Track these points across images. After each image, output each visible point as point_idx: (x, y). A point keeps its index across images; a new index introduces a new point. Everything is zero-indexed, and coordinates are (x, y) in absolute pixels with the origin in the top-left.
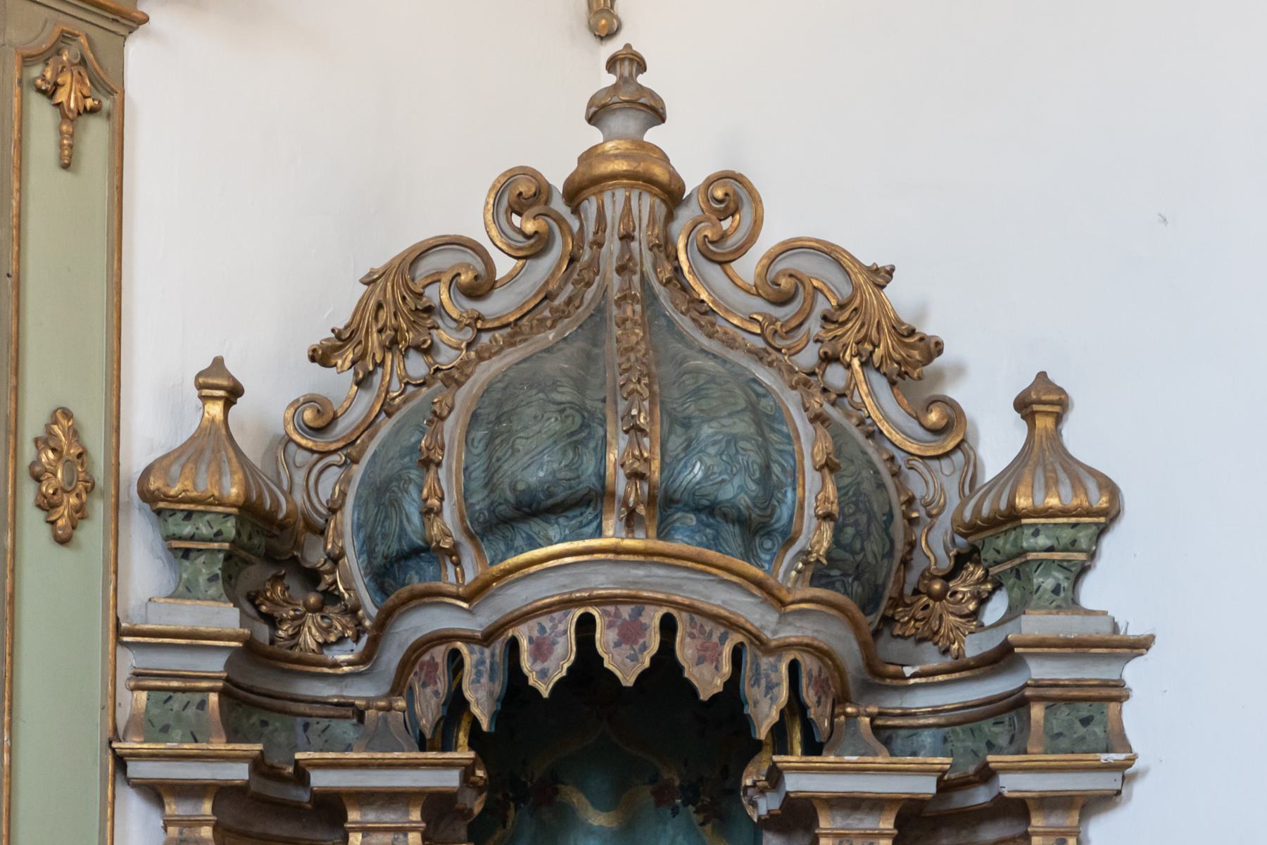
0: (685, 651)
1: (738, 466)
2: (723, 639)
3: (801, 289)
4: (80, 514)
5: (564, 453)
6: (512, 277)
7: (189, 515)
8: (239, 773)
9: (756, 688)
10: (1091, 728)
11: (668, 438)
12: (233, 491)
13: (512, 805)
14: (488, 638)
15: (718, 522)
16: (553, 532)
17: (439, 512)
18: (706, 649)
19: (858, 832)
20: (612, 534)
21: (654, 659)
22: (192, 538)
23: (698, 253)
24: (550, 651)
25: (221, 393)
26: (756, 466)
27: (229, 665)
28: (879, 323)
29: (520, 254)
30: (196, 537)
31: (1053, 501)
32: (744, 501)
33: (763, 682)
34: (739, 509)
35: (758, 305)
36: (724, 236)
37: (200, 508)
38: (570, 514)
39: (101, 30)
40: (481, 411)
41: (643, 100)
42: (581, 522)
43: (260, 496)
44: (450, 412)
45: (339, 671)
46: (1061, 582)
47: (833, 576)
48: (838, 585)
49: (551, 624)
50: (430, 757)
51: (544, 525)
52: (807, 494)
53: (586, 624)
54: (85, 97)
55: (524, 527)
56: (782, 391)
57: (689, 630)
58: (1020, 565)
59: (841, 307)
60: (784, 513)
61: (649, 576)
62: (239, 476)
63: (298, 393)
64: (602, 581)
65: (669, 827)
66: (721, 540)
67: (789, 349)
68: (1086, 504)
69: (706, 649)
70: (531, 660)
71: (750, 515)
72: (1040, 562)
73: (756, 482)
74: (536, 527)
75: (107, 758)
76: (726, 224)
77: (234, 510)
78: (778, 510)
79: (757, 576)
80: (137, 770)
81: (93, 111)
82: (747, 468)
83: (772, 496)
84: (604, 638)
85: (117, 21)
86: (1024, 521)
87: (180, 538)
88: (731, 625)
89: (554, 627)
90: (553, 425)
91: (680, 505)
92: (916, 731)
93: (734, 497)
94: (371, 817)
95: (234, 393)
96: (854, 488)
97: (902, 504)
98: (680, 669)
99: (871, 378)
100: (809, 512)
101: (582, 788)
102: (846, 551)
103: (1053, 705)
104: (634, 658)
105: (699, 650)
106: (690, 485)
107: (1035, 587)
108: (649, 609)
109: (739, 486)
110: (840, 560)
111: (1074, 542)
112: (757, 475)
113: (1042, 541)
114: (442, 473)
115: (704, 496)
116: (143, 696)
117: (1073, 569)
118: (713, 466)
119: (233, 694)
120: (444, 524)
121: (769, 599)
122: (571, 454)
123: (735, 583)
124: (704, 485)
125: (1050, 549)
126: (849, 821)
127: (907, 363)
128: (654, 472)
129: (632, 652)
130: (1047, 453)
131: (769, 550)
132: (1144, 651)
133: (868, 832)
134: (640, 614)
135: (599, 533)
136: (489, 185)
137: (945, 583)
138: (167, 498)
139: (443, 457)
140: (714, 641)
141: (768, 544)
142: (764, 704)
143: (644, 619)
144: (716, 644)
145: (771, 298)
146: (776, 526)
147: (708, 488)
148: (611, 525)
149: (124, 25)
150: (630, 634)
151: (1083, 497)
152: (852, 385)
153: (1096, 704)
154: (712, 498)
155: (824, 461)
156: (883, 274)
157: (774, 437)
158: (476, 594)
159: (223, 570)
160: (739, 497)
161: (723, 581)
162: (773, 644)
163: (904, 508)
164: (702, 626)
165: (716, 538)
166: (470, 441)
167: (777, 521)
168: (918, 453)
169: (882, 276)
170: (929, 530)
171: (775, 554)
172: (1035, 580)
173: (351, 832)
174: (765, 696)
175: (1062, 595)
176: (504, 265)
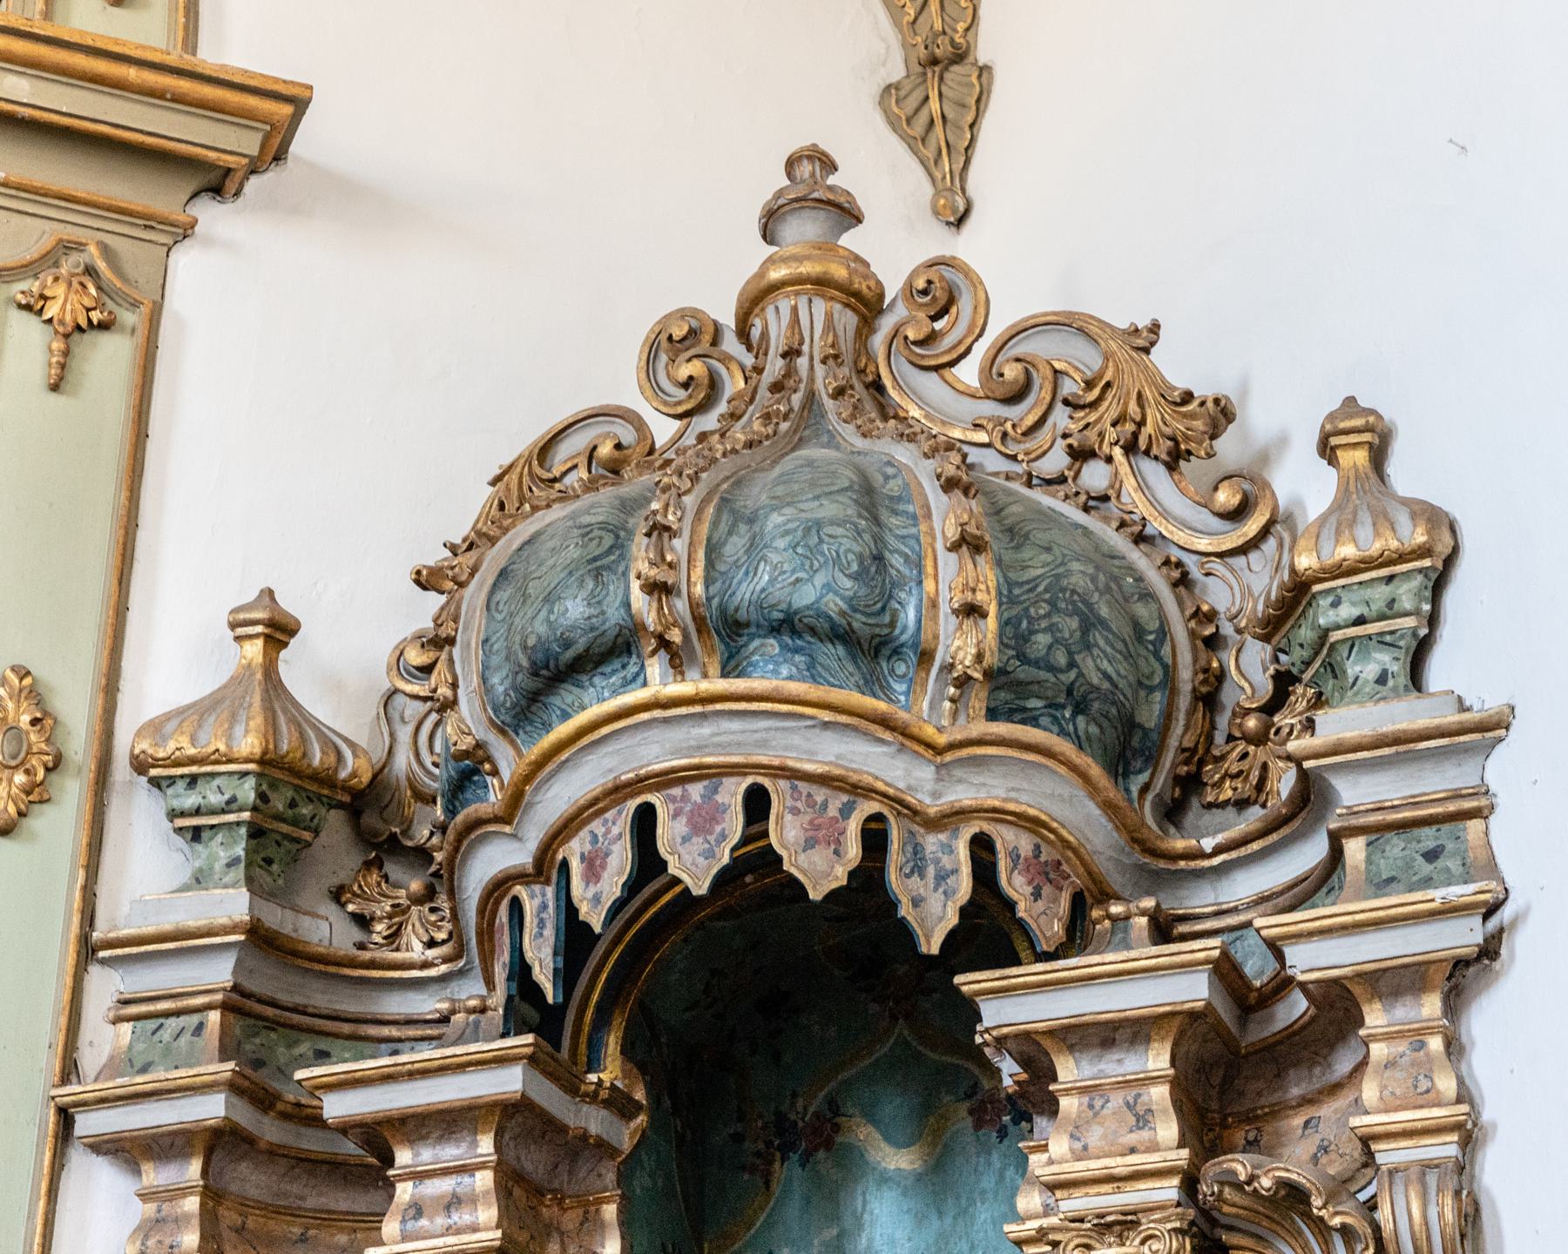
0: (785, 833)
1: (822, 560)
2: (846, 811)
3: (1035, 374)
5: (581, 582)
7: (193, 780)
9: (916, 878)
10: (1440, 863)
11: (726, 541)
12: (249, 743)
13: (778, 1155)
15: (809, 642)
18: (818, 828)
19: (1114, 1079)
22: (198, 812)
23: (915, 371)
24: (603, 867)
25: (259, 629)
26: (851, 556)
27: (239, 965)
28: (1140, 396)
29: (680, 410)
30: (203, 810)
31: (1348, 551)
32: (834, 605)
33: (931, 871)
34: (830, 617)
35: (990, 408)
37: (209, 769)
38: (607, 669)
39: (126, 239)
40: (515, 566)
41: (815, 195)
42: (625, 677)
44: (472, 575)
45: (433, 972)
46: (1388, 666)
47: (1031, 709)
48: (1044, 721)
49: (603, 830)
50: (472, 1050)
51: (576, 690)
52: (940, 587)
53: (645, 821)
54: (88, 310)
55: (556, 700)
56: (916, 464)
57: (789, 803)
58: (1328, 655)
61: (718, 734)
62: (258, 721)
65: (995, 1157)
66: (819, 669)
67: (1027, 454)
68: (1394, 544)
69: (818, 828)
70: (583, 884)
71: (849, 624)
72: (1352, 642)
73: (855, 577)
74: (566, 695)
75: (47, 1114)
76: (938, 325)
77: (252, 767)
78: (902, 615)
79: (876, 710)
80: (88, 1124)
81: (104, 326)
82: (837, 561)
83: (891, 597)
84: (668, 832)
85: (153, 228)
86: (1316, 588)
88: (859, 790)
89: (608, 831)
90: (573, 553)
91: (753, 630)
92: (1239, 933)
93: (817, 601)
94: (428, 1155)
95: (280, 631)
96: (1048, 581)
97: (1189, 620)
98: (893, 905)
99: (1142, 468)
100: (944, 608)
101: (872, 1120)
102: (1039, 668)
103: (1377, 839)
105: (806, 830)
106: (755, 595)
107: (1351, 680)
109: (824, 586)
110: (1032, 683)
112: (855, 567)
113: (1347, 611)
114: (457, 652)
115: (772, 606)
116: (126, 1028)
117: (1402, 643)
118: (782, 563)
119: (238, 1003)
120: (462, 721)
121: (908, 743)
122: (590, 584)
123: (847, 726)
124: (771, 590)
125: (1360, 621)
126: (1102, 1066)
127: (1187, 438)
128: (695, 584)
129: (707, 846)
130: (1354, 496)
131: (904, 676)
132: (1502, 732)
133: (1128, 1077)
134: (716, 791)
136: (643, 338)
137: (1267, 718)
139: (456, 631)
140: (831, 815)
141: (901, 668)
142: (935, 902)
143: (719, 798)
145: (998, 395)
146: (904, 638)
148: (656, 668)
149: (161, 230)
151: (1388, 533)
152: (1116, 482)
153: (1446, 827)
154: (783, 606)
155: (957, 536)
156: (1145, 334)
157: (894, 521)
158: (516, 803)
159: (246, 850)
160: (825, 600)
161: (826, 725)
162: (932, 811)
163: (1192, 624)
164: (809, 795)
165: (811, 666)
166: (493, 606)
167: (902, 633)
168: (1210, 549)
169: (1145, 339)
170: (1239, 651)
171: (911, 679)
172: (1349, 671)
173: (399, 1181)
174: (936, 889)
175: (1391, 683)
176: (663, 429)
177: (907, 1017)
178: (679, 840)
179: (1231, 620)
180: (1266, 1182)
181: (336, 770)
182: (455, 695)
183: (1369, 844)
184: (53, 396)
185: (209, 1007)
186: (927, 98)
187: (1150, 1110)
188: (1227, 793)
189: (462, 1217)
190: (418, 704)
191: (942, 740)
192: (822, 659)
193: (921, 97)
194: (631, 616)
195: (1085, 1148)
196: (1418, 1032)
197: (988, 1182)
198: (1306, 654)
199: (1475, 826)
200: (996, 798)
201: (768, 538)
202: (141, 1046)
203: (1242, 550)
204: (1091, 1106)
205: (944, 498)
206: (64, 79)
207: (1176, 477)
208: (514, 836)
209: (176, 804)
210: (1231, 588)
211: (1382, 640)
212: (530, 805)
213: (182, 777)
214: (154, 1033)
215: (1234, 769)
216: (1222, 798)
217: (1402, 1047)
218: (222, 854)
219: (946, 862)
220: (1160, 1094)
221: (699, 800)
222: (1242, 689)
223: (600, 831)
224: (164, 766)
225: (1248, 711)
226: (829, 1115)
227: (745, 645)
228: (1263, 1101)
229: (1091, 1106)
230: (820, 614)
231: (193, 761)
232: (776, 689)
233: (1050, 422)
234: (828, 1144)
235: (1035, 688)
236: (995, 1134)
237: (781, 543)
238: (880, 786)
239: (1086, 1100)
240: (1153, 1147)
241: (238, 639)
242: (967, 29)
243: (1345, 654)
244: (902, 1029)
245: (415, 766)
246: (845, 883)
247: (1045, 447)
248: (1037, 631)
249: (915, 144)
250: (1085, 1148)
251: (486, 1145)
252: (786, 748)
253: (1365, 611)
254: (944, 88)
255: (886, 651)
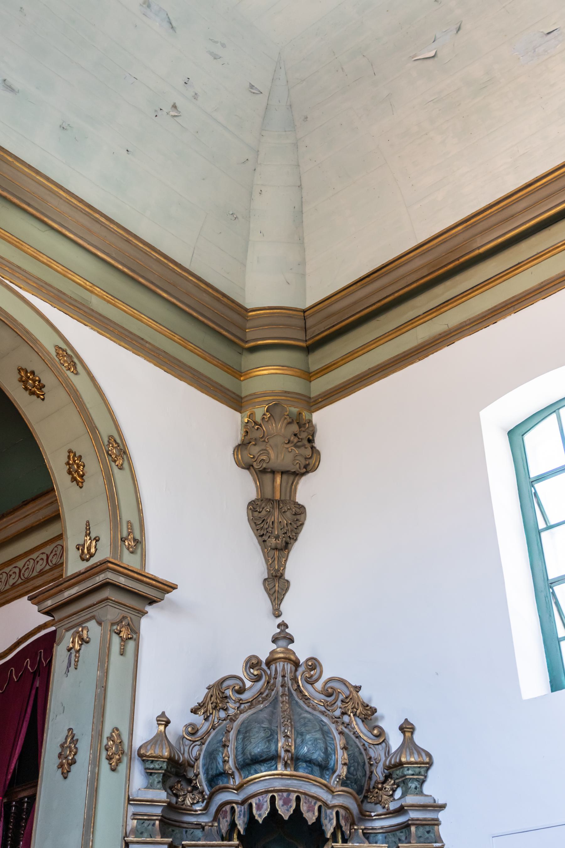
0: (304, 808)
2: (315, 804)
4: (119, 761)
6: (251, 687)
7: (152, 762)
12: (166, 754)
14: (243, 803)
16: (263, 768)
20: (280, 770)
21: (294, 811)
22: (153, 769)
24: (262, 808)
25: (164, 723)
27: (162, 811)
28: (358, 703)
29: (253, 681)
32: (320, 759)
33: (328, 818)
35: (322, 697)
36: (312, 676)
37: (156, 759)
38: (268, 763)
41: (287, 637)
43: (174, 755)
51: (259, 766)
53: (273, 798)
54: (129, 635)
59: (347, 698)
60: (332, 763)
62: (168, 749)
63: (187, 722)
64: (278, 785)
67: (332, 710)
72: (410, 779)
73: (323, 753)
74: (257, 767)
77: (166, 760)
78: (330, 762)
81: (131, 638)
84: (279, 803)
87: (149, 769)
88: (317, 799)
89: (263, 800)
91: (300, 760)
93: (317, 758)
100: (339, 762)
108: (292, 794)
111: (420, 772)
113: (410, 772)
115: (308, 757)
116: (135, 821)
122: (267, 744)
125: (413, 775)
132: (444, 808)
135: (276, 769)
138: (146, 756)
141: (328, 773)
142: (329, 825)
143: (291, 797)
146: (330, 767)
148: (280, 766)
150: (286, 802)
151: (421, 758)
153: (431, 826)
154: (310, 758)
155: (343, 746)
158: (239, 788)
159: (162, 779)
162: (331, 805)
164: (308, 799)
165: (312, 770)
168: (371, 743)
169: (358, 689)
170: (376, 767)
175: (418, 789)
176: (248, 684)
178: (281, 806)
179: (375, 760)
182: (229, 759)
184: (121, 657)
186: (275, 586)
190: (189, 741)
193: (274, 585)
194: (277, 754)
198: (398, 777)
199: (436, 827)
200: (341, 803)
202: (139, 827)
203: (378, 744)
205: (339, 736)
206: (131, 579)
208: (237, 794)
209: (147, 766)
212: (244, 789)
213: (150, 760)
214: (142, 823)
216: (372, 801)
218: (156, 779)
222: (377, 777)
223: (261, 799)
224: (147, 757)
227: (298, 763)
230: (317, 761)
232: (307, 776)
233: (336, 703)
237: (310, 743)
238: (323, 800)
242: (283, 569)
246: (315, 821)
249: (270, 595)
253: (414, 773)
254: (279, 585)
255: (326, 769)
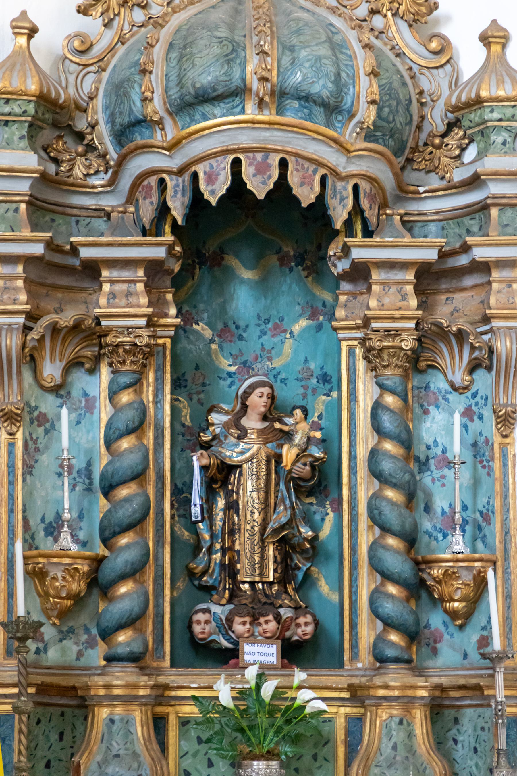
2: (315, 172)
7: (7, 101)
8: (38, 249)
12: (33, 87)
13: (198, 266)
14: (180, 172)
16: (217, 111)
17: (151, 100)
22: (9, 114)
24: (216, 179)
25: (26, 31)
26: (332, 74)
27: (31, 187)
30: (12, 114)
31: (501, 93)
32: (325, 93)
33: (338, 197)
38: (226, 101)
43: (49, 90)
45: (96, 190)
48: (380, 141)
58: (484, 129)
60: (348, 100)
62: (36, 79)
67: (351, 6)
70: (206, 184)
72: (495, 127)
74: (207, 108)
77: (34, 98)
78: (345, 98)
83: (342, 91)
86: (485, 104)
88: (319, 164)
89: (218, 165)
90: (216, 50)
91: (289, 96)
94: (115, 274)
100: (362, 99)
101: (237, 256)
104: (264, 183)
107: (492, 142)
108: (272, 154)
112: (333, 78)
113: (496, 115)
115: (302, 91)
117: (513, 131)
120: (154, 107)
122: (226, 67)
125: (500, 120)
126: (389, 275)
131: (340, 121)
135: (243, 111)
141: (340, 118)
142: (339, 209)
143: (269, 161)
144: (311, 175)
146: (344, 107)
147: (304, 87)
152: (387, 26)
154: (307, 92)
157: (341, 57)
159: (28, 132)
161: (314, 139)
162: (344, 174)
164: (302, 164)
167: (344, 105)
168: (425, 65)
170: (432, 109)
174: (340, 204)
175: (507, 145)
177: (252, 217)
178: (251, 175)
179: (430, 96)
180: (454, 329)
181: (58, 99)
183: (500, 210)
185: (22, 201)
187: (406, 294)
188: (422, 166)
189: (133, 300)
190: (76, 66)
191: (352, 149)
192: (314, 112)
194: (245, 85)
195: (383, 305)
196: (510, 281)
197: (285, 288)
201: (301, 61)
203: (437, 68)
204: (384, 290)
205: (363, 51)
207: (412, 30)
210: (430, 82)
211: (507, 129)
215: (427, 157)
216: (421, 168)
217: (503, 285)
219: (344, 193)
220: (410, 289)
221: (260, 160)
225: (435, 136)
226: (220, 253)
228: (429, 288)
229: (384, 290)
231: (10, 93)
232: (300, 123)
234: (219, 265)
235: (381, 129)
236: (288, 270)
237: (307, 65)
238: (329, 165)
239: (382, 287)
240: (408, 309)
241: (16, 34)
243: (491, 131)
244: (250, 220)
245: (77, 95)
247: (358, 4)
248: (385, 107)
250: (383, 305)
251: (141, 273)
252: (296, 145)
253: (503, 117)
255: (336, 111)
